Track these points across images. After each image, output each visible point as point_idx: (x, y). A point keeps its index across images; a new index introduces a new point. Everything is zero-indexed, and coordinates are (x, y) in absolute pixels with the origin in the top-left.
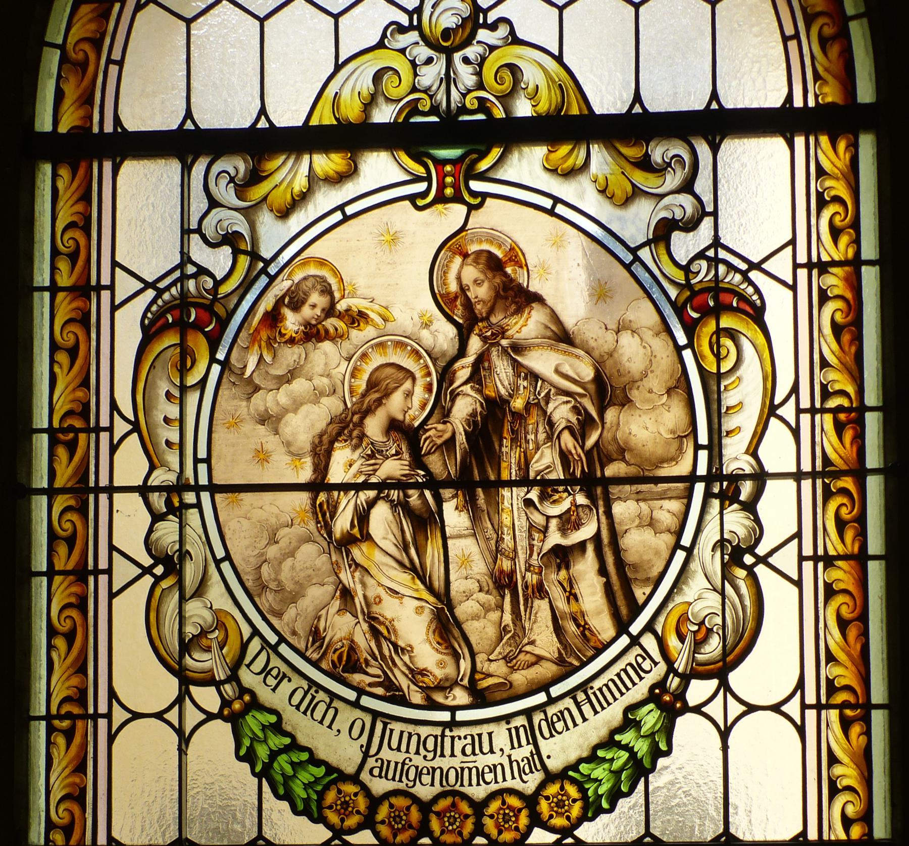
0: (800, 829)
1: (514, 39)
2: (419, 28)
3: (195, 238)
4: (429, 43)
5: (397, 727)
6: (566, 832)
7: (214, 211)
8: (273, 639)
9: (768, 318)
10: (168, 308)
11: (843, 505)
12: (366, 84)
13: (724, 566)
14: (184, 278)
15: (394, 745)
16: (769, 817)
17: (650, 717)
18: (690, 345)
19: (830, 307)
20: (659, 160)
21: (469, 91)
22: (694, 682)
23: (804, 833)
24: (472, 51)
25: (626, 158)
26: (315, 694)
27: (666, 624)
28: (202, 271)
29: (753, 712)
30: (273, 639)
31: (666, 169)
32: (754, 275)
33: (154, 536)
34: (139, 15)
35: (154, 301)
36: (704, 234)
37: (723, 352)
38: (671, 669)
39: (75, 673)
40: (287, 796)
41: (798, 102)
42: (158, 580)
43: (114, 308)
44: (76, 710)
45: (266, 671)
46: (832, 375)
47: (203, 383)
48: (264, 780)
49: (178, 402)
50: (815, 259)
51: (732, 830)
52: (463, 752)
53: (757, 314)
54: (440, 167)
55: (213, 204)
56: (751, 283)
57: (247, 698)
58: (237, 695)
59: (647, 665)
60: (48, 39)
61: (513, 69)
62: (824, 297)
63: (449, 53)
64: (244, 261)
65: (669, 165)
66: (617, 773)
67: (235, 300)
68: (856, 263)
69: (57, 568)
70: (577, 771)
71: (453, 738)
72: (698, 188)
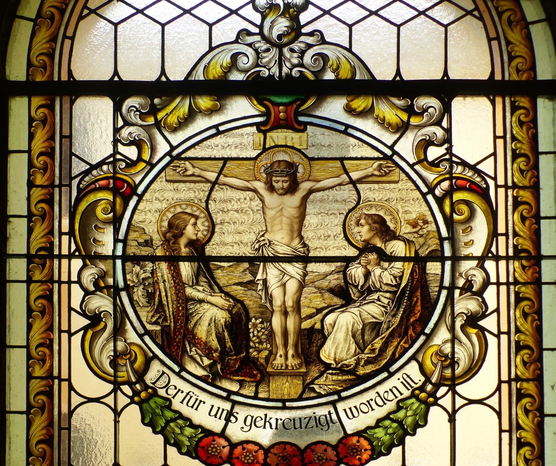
1: (323, 41)
2: (261, 33)
12: (226, 60)
24: (296, 46)
25: (394, 104)
40: (178, 445)
41: (498, 77)
54: (276, 108)
57: (150, 390)
58: (144, 389)
61: (324, 57)
63: (280, 47)
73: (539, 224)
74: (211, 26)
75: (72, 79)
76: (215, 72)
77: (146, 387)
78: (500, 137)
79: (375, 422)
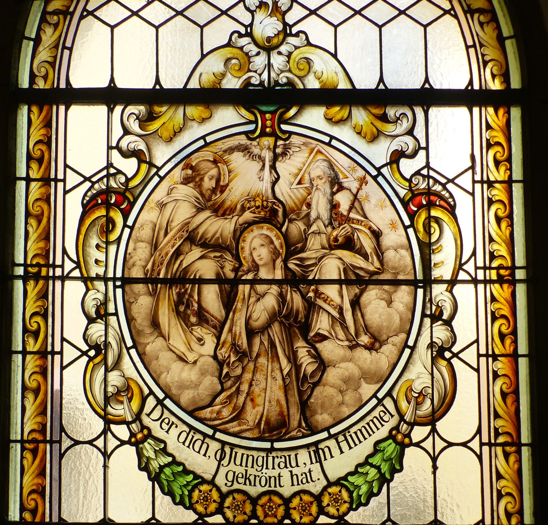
0: (480, 518)
1: (309, 44)
2: (249, 34)
3: (115, 152)
5: (240, 451)
9: (457, 212)
10: (100, 193)
11: (500, 153)
13: (433, 359)
14: (108, 176)
15: (238, 462)
16: (459, 504)
17: (391, 448)
18: (412, 225)
19: (499, 382)
21: (282, 72)
22: (416, 427)
24: (284, 49)
26: (193, 435)
27: (399, 392)
28: (119, 172)
29: (451, 446)
30: (161, 395)
31: (397, 122)
32: (450, 186)
33: (89, 332)
35: (89, 190)
36: (420, 160)
39: (40, 414)
40: (170, 493)
42: (91, 359)
43: (66, 192)
45: (161, 419)
47: (119, 238)
48: (156, 482)
49: (105, 250)
50: (485, 178)
53: (451, 210)
56: (448, 191)
57: (145, 432)
60: (27, 35)
61: (308, 61)
64: (144, 167)
65: (398, 119)
66: (371, 483)
68: (509, 183)
69: (28, 350)
70: (347, 480)
74: (336, 27)
76: (207, 80)
77: (143, 427)
79: (354, 467)
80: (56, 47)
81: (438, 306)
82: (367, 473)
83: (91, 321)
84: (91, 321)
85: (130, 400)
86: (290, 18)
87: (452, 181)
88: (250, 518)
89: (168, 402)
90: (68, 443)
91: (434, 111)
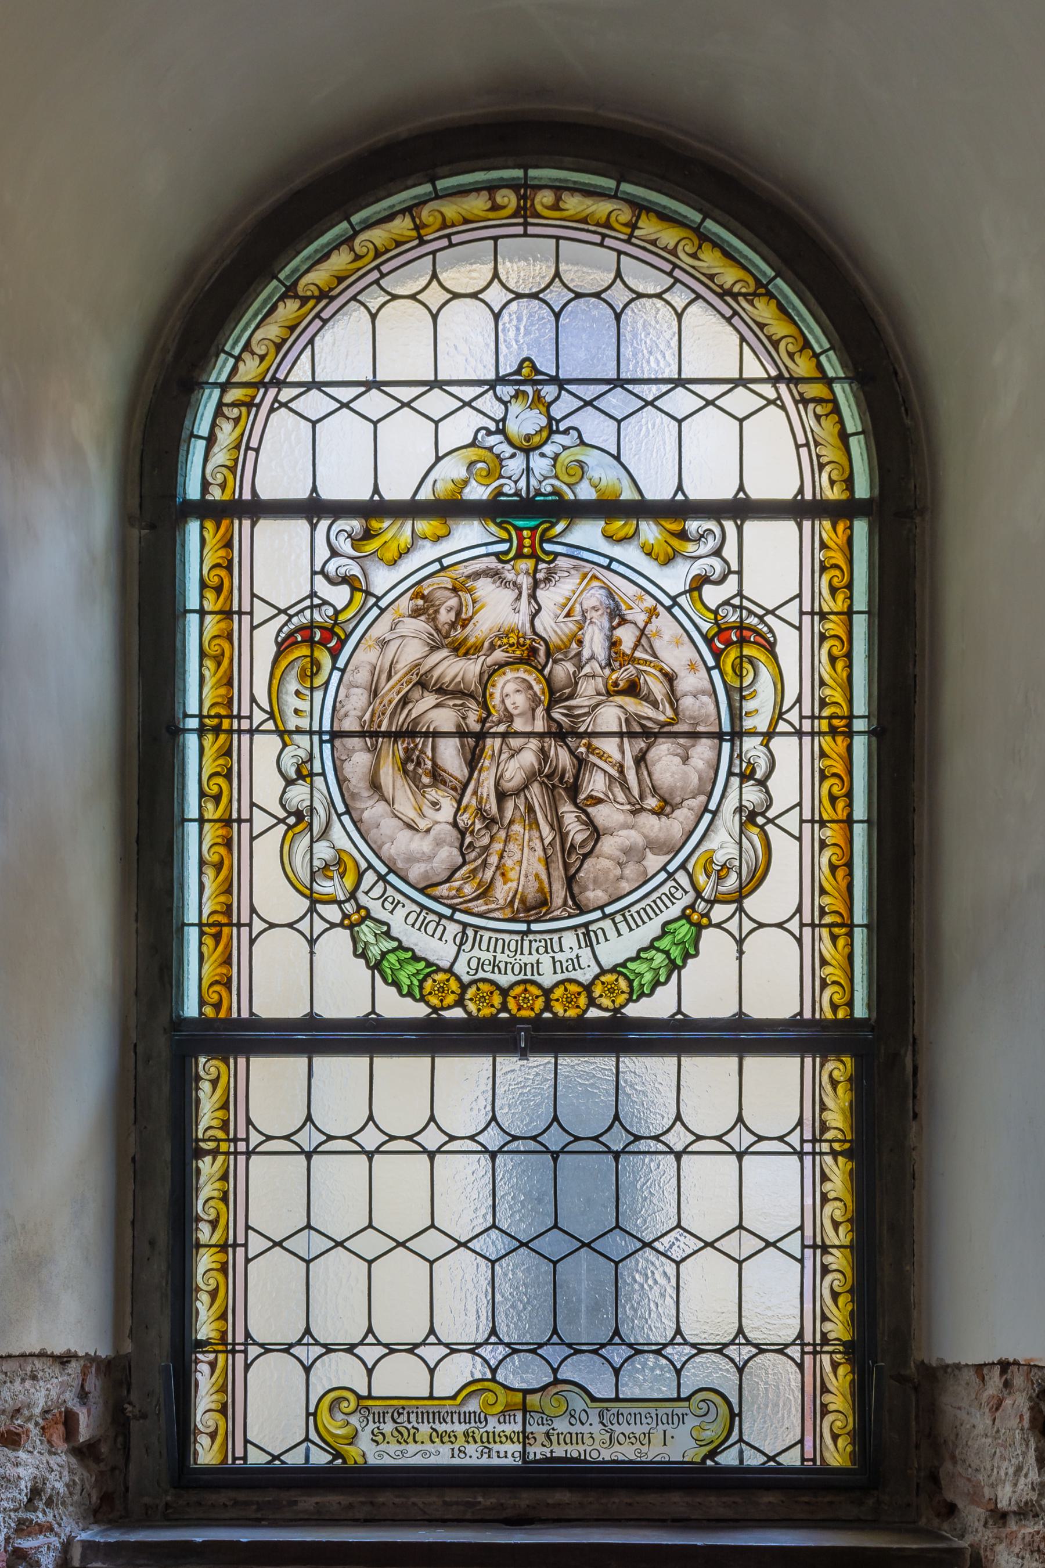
1: (582, 443)
2: (502, 432)
3: (319, 578)
4: (511, 444)
6: (616, 1010)
7: (334, 560)
8: (383, 870)
9: (778, 650)
13: (741, 824)
14: (312, 607)
17: (684, 930)
18: (717, 666)
19: (827, 853)
20: (694, 532)
21: (546, 478)
23: (801, 1013)
28: (325, 602)
30: (383, 870)
31: (699, 540)
32: (769, 619)
33: (286, 796)
34: (272, 416)
35: (285, 624)
37: (744, 673)
38: (699, 894)
40: (396, 984)
42: (290, 828)
44: (224, 920)
46: (828, 691)
47: (327, 683)
51: (744, 1010)
52: (537, 950)
53: (770, 648)
55: (334, 553)
56: (767, 625)
57: (363, 913)
59: (678, 895)
61: (581, 464)
62: (823, 845)
65: (702, 536)
66: (656, 970)
67: (351, 626)
70: (625, 967)
71: (530, 941)
72: (725, 553)
73: (852, 739)
75: (739, 522)
76: (444, 490)
77: (359, 907)
78: (802, 446)
80: (238, 447)
81: (749, 762)
82: (652, 959)
83: (289, 782)
84: (289, 782)
85: (342, 875)
86: (557, 412)
87: (772, 612)
88: (499, 1011)
89: (391, 878)
90: (257, 1350)
91: (751, 527)
